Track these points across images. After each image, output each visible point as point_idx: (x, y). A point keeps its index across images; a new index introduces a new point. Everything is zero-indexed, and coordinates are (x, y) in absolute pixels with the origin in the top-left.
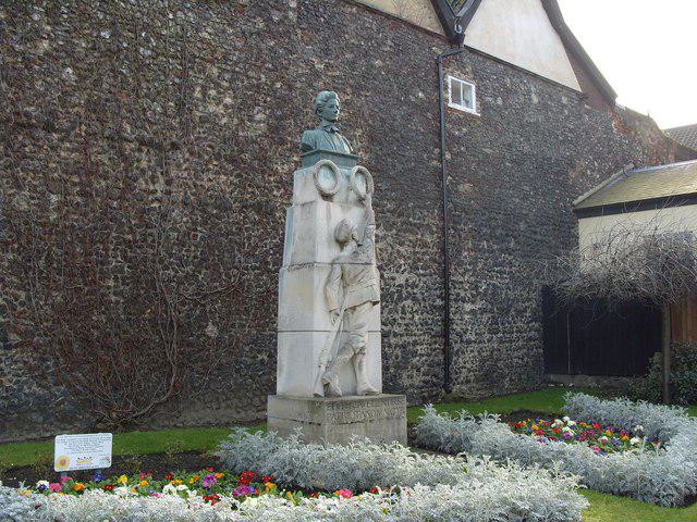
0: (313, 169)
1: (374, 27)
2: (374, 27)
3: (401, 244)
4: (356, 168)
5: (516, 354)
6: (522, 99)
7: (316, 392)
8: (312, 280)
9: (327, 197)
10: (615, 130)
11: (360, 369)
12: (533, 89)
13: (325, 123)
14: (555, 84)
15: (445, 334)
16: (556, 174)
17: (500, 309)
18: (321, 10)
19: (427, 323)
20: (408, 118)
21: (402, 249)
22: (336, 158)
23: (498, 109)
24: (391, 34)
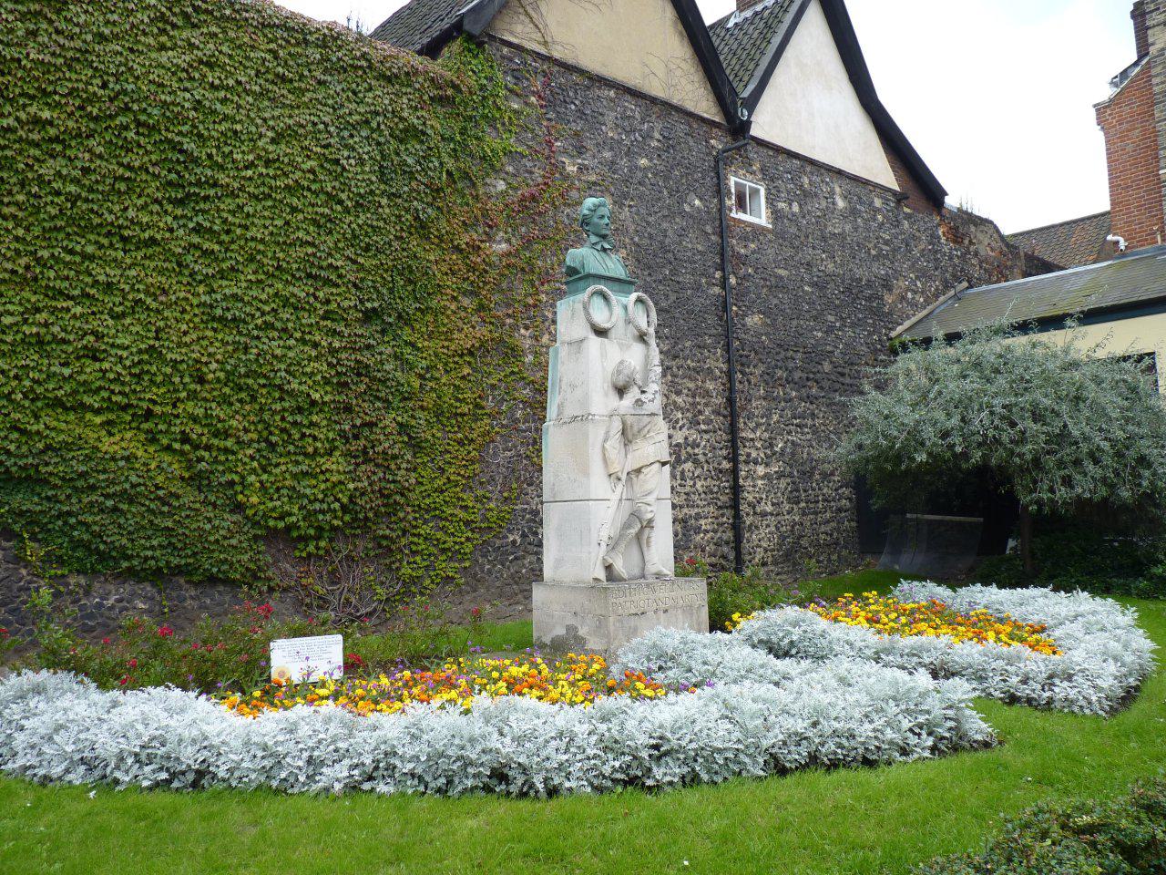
0: (584, 296)
1: (637, 115)
2: (637, 115)
3: (678, 393)
4: (634, 296)
5: (823, 528)
6: (824, 204)
7: (596, 576)
8: (586, 436)
9: (601, 332)
10: (943, 240)
11: (648, 543)
12: (838, 190)
13: (594, 239)
14: (866, 183)
15: (735, 505)
16: (869, 299)
17: (802, 473)
18: (571, 94)
19: (712, 492)
20: (682, 234)
21: (679, 400)
22: (610, 283)
23: (793, 219)
24: (658, 126)
